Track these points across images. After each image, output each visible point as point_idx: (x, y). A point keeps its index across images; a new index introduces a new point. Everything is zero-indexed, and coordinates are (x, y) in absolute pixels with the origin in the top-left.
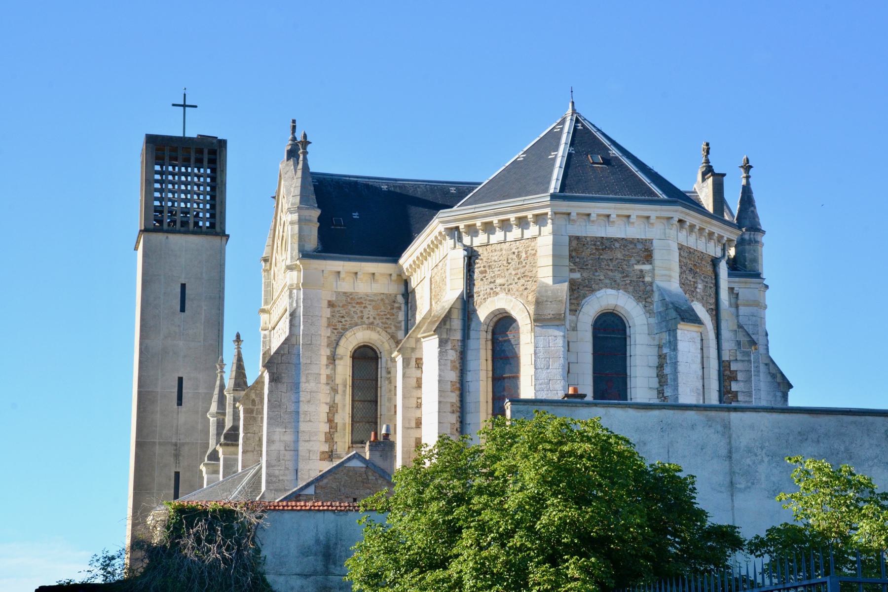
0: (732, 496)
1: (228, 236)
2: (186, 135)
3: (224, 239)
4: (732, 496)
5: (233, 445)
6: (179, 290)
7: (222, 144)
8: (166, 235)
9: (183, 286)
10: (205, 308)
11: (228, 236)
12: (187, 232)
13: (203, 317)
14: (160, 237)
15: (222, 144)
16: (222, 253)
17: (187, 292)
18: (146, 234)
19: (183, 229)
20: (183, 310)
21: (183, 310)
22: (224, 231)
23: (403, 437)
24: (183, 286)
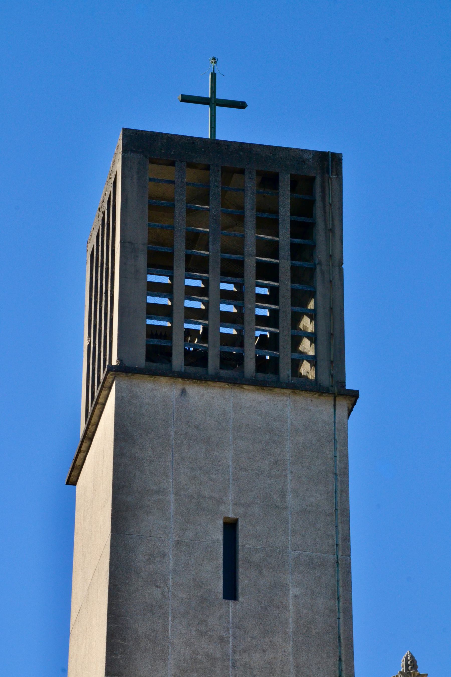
0: (335, 406)
1: (354, 396)
2: (219, 136)
3: (343, 404)
4: (335, 406)
5: (270, 371)
6: (219, 536)
7: (330, 163)
8: (179, 384)
9: (231, 528)
10: (294, 591)
11: (354, 396)
12: (238, 381)
13: (291, 616)
14: (160, 391)
15: (330, 163)
16: (337, 439)
17: (241, 541)
18: (125, 381)
19: (224, 373)
20: (231, 592)
21: (231, 592)
22: (343, 384)
23: (121, 241)
24: (231, 528)
